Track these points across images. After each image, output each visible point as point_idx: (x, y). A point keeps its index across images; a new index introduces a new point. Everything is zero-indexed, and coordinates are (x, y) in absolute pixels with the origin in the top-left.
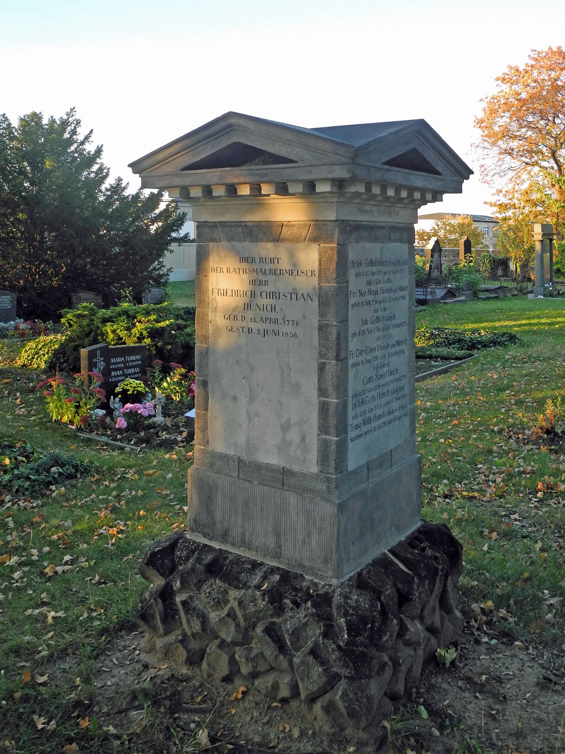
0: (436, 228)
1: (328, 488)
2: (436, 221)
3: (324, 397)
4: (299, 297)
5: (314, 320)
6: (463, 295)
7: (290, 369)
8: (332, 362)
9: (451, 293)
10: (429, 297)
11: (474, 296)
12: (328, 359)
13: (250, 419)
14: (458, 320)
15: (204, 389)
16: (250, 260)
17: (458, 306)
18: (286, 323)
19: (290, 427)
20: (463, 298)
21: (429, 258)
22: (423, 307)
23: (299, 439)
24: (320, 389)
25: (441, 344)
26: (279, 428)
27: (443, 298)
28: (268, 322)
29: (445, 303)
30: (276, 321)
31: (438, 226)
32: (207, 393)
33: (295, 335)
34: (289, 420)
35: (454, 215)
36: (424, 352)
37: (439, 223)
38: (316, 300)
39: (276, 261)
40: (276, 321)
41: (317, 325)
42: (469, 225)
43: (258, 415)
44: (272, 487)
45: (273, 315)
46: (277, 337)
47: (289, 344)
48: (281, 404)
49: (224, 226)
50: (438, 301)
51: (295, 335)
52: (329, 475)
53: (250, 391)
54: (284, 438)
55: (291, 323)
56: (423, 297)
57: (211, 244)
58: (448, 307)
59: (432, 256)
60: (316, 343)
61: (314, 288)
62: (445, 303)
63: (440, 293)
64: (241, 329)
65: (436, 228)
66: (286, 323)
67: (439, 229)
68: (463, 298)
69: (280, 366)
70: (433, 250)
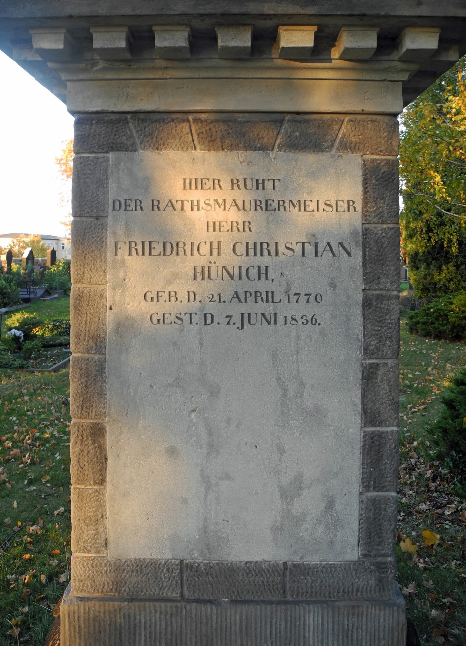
0: (12, 245)
1: (380, 580)
2: (12, 239)
3: (373, 426)
4: (320, 249)
5: (356, 289)
6: (56, 293)
7: (302, 384)
8: (389, 361)
9: (48, 292)
10: (32, 296)
11: (65, 294)
12: (382, 358)
13: (209, 487)
14: (60, 313)
15: (94, 442)
16: (210, 184)
17: (55, 302)
18: (293, 299)
19: (300, 489)
20: (56, 296)
21: (24, 265)
22: (28, 305)
23: (322, 506)
24: (365, 411)
25: (64, 333)
26: (277, 493)
27: (42, 296)
28: (251, 299)
29: (44, 300)
30: (270, 297)
31: (14, 243)
32: (102, 449)
33: (313, 321)
34: (299, 479)
35: (27, 235)
36: (55, 341)
37: (15, 241)
38: (358, 253)
39: (269, 185)
40: (270, 297)
41: (360, 297)
42: (38, 242)
43: (228, 477)
44: (263, 602)
45: (263, 286)
46: (272, 327)
47: (298, 337)
48: (281, 450)
49: (144, 121)
50: (38, 299)
51: (313, 321)
52: (379, 559)
53: (210, 433)
54: (289, 510)
55: (303, 299)
56: (27, 296)
57: (111, 155)
58: (47, 303)
59: (27, 263)
60: (358, 330)
61: (354, 233)
62: (44, 300)
63: (40, 292)
64: (186, 318)
65: (12, 245)
66: (293, 299)
67: (14, 245)
68: (56, 296)
69: (279, 379)
70: (28, 259)
